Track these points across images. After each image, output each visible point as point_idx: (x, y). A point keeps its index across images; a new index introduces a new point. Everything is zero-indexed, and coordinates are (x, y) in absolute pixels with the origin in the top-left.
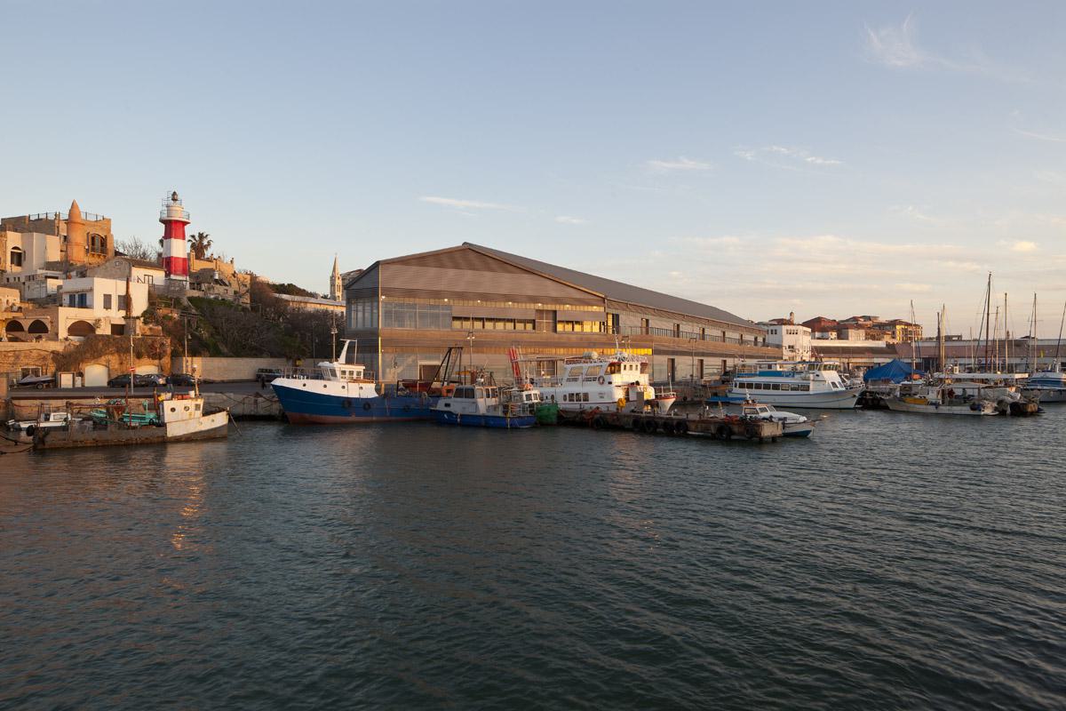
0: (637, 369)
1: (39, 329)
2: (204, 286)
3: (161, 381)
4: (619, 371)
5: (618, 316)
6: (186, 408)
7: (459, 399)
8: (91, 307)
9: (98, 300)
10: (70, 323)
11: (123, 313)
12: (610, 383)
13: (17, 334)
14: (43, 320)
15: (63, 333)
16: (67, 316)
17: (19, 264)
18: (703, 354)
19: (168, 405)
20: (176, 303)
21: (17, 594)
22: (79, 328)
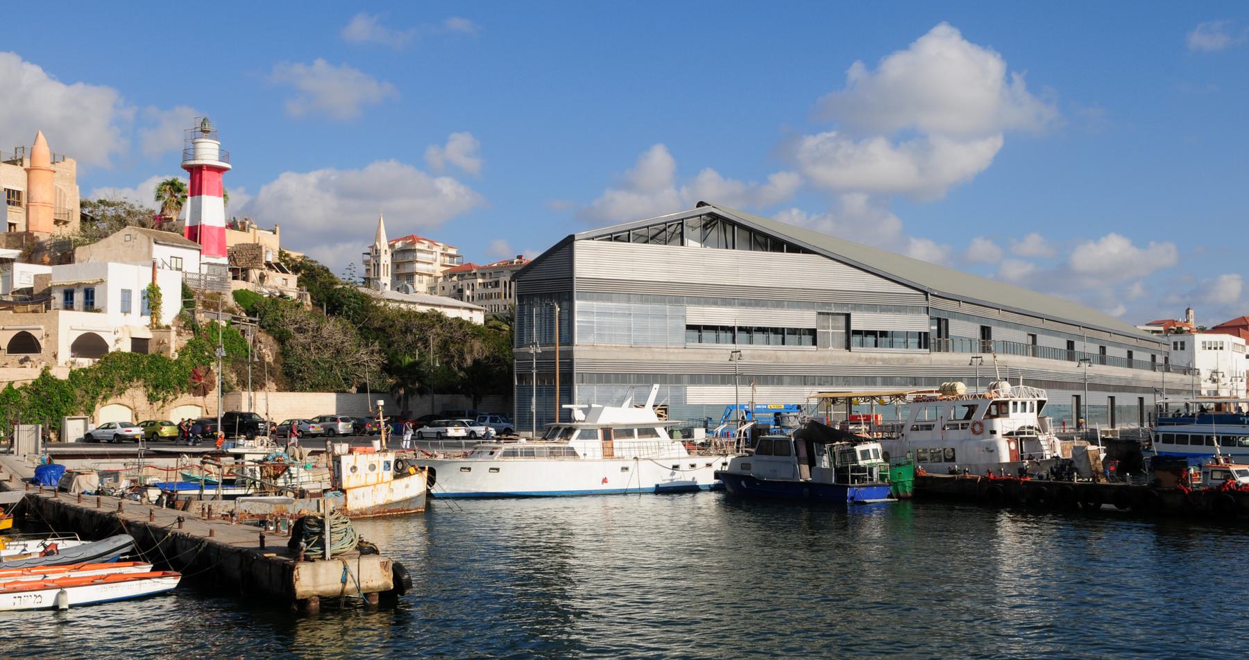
0: (1032, 411)
2: (254, 274)
3: (342, 427)
4: (1006, 414)
5: (989, 329)
6: (373, 467)
7: (765, 457)
9: (111, 297)
10: (74, 336)
12: (994, 432)
14: (33, 332)
16: (71, 323)
18: (1081, 386)
19: (347, 462)
21: (897, 594)
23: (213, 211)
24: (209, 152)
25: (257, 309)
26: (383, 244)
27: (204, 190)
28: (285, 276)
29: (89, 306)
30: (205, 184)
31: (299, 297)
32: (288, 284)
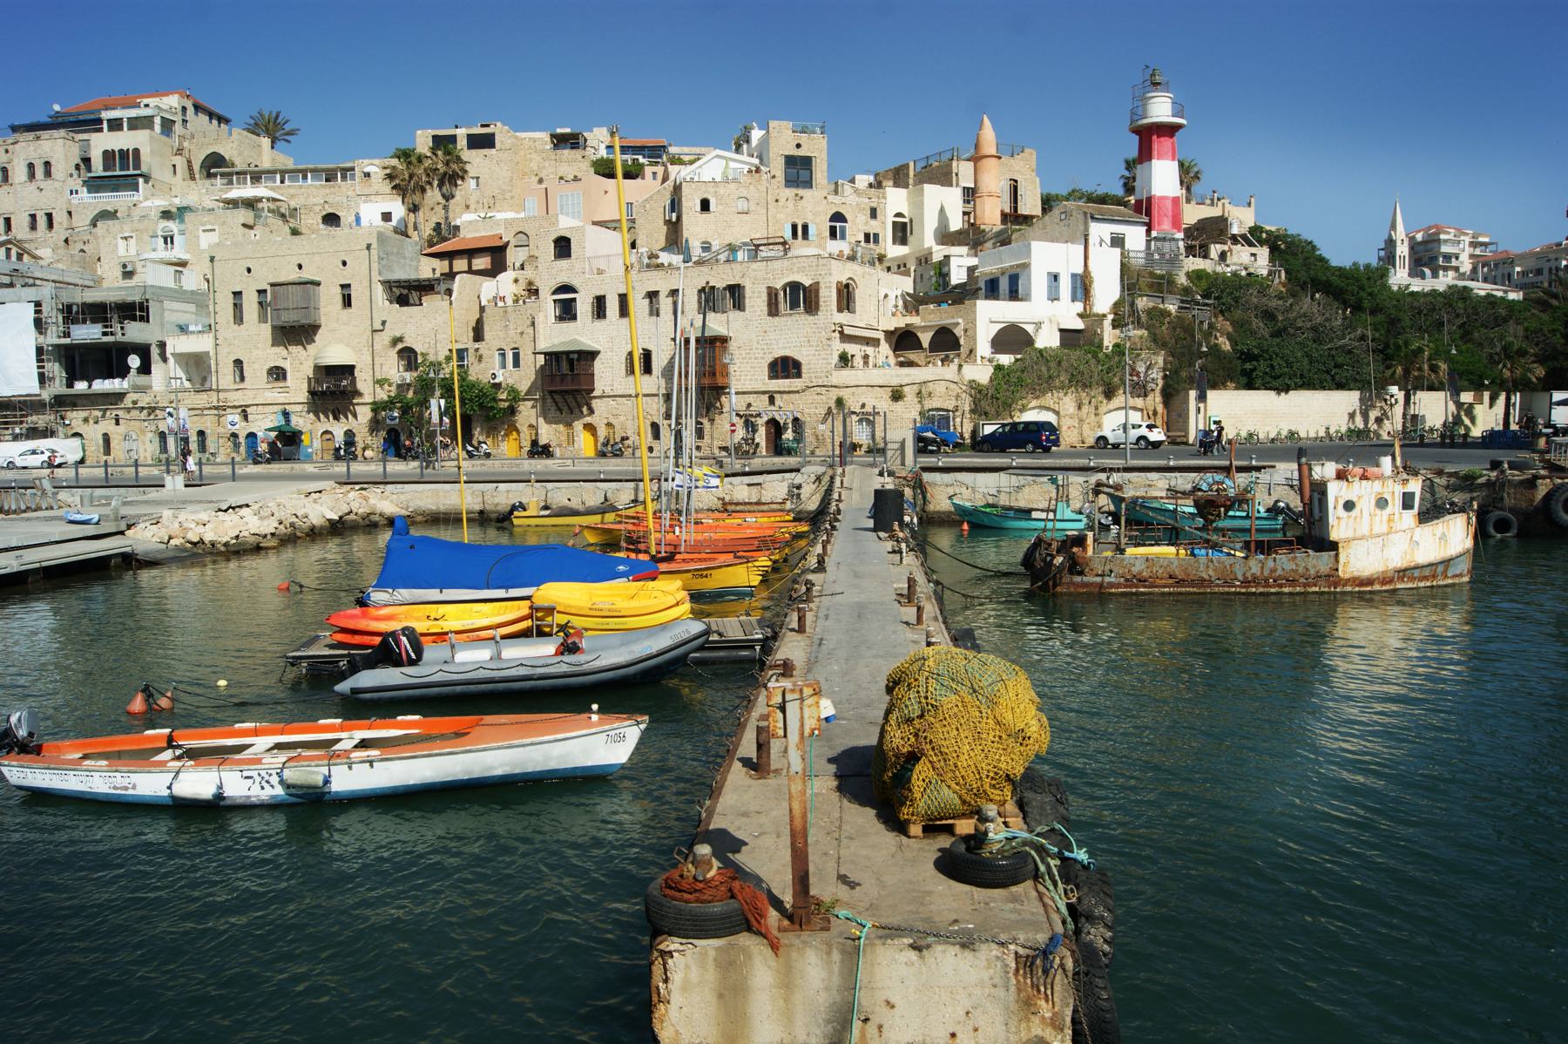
1: (946, 342)
2: (1215, 250)
6: (1382, 503)
8: (1027, 298)
9: (1038, 283)
11: (1079, 307)
13: (912, 355)
15: (984, 348)
16: (990, 315)
17: (904, 241)
20: (1162, 285)
22: (1012, 338)
23: (1163, 178)
24: (1161, 109)
25: (1224, 293)
26: (1400, 234)
27: (1155, 153)
28: (1253, 250)
29: (1014, 295)
30: (1155, 146)
31: (1270, 273)
32: (1257, 261)
